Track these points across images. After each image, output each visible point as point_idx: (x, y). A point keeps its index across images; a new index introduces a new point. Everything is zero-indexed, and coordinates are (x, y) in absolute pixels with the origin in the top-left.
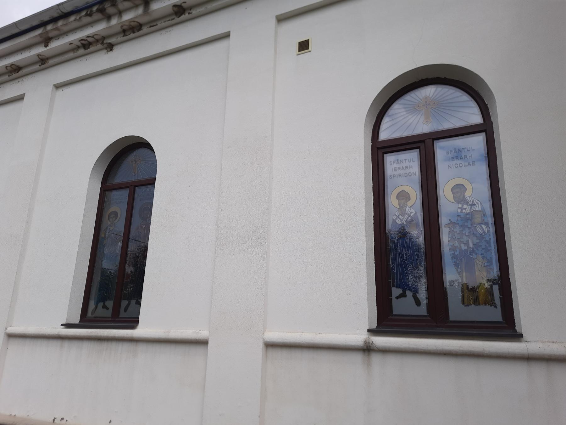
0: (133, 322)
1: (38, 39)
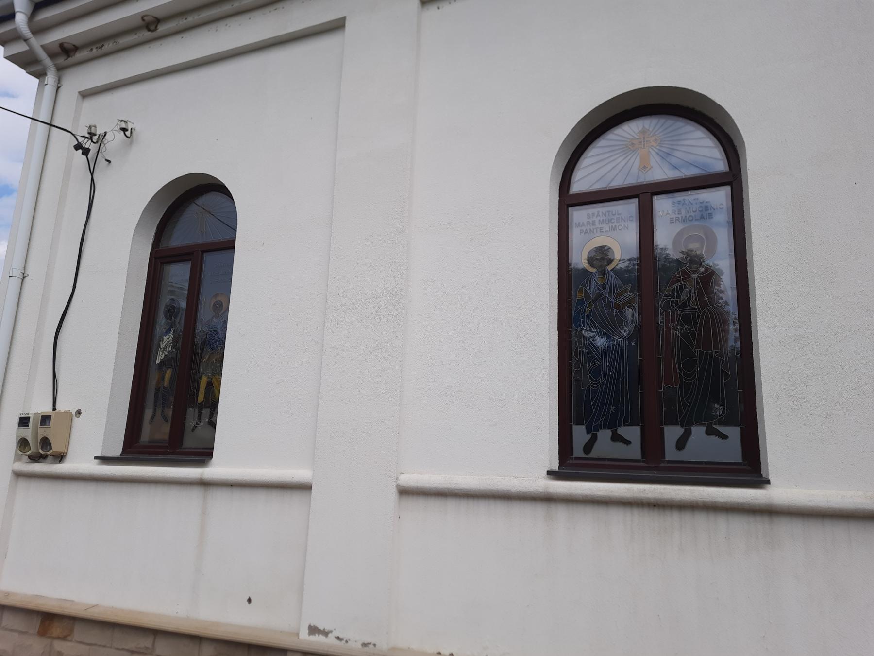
0: (203, 454)
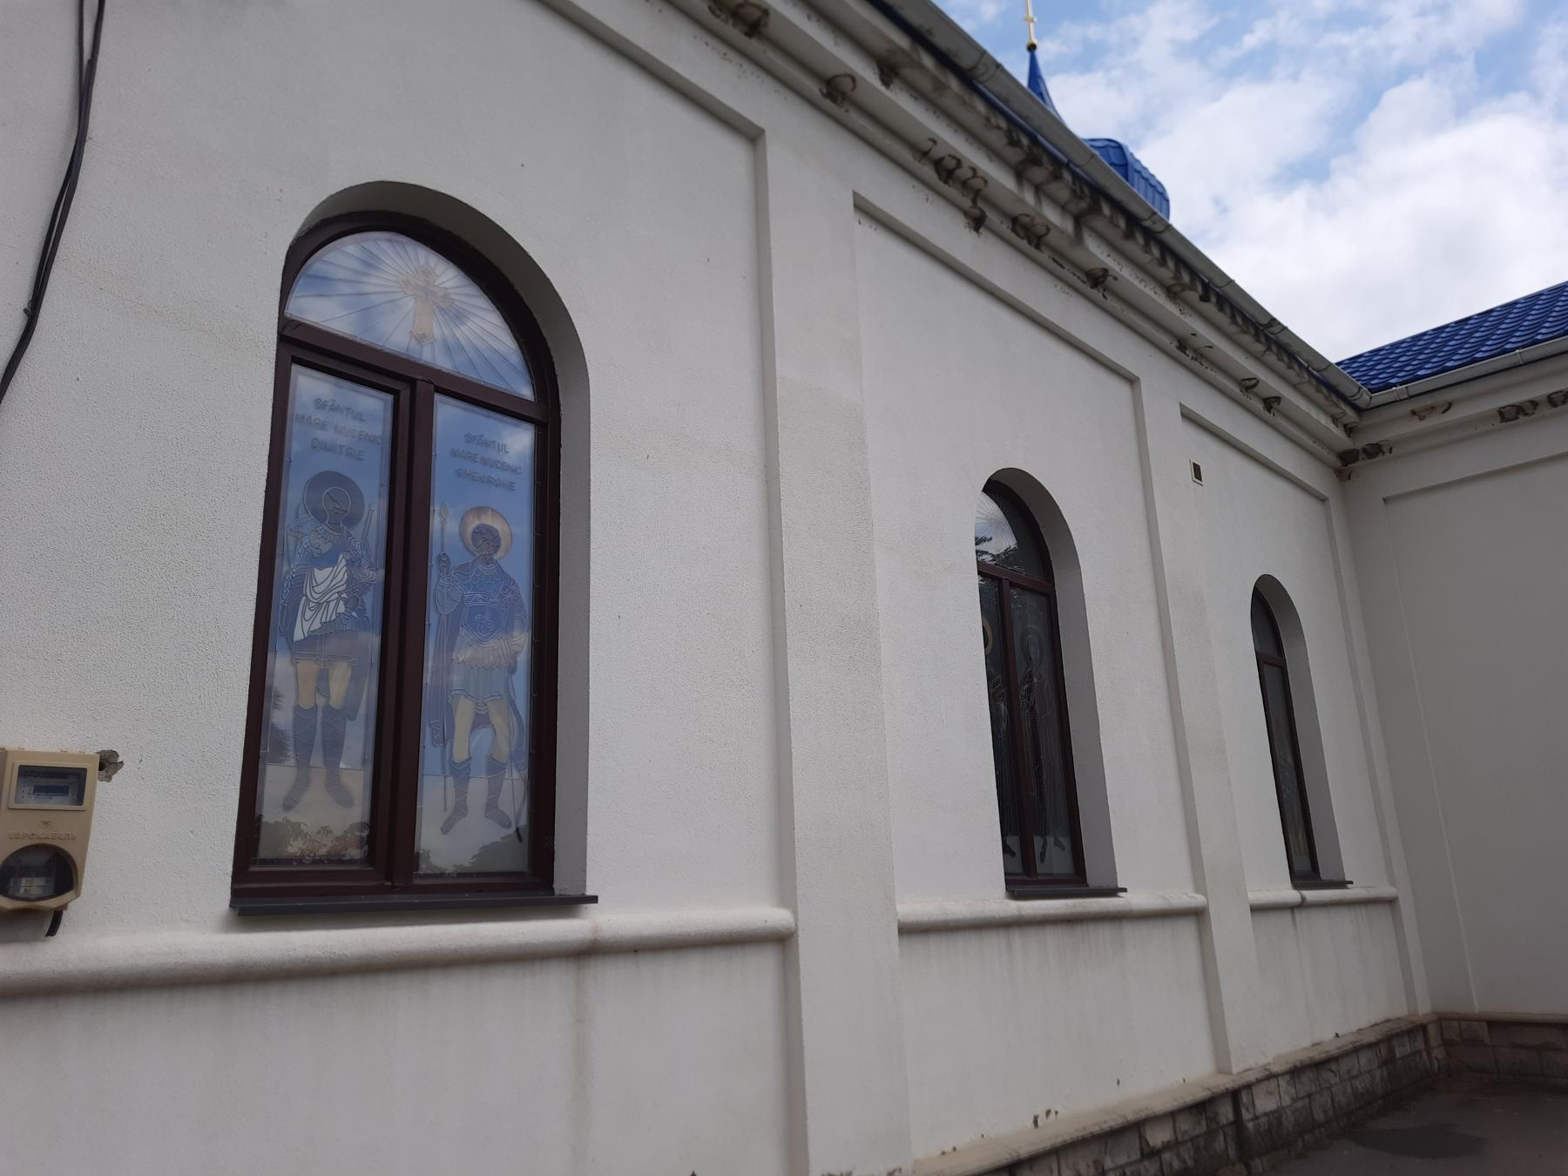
1: (881, 47)
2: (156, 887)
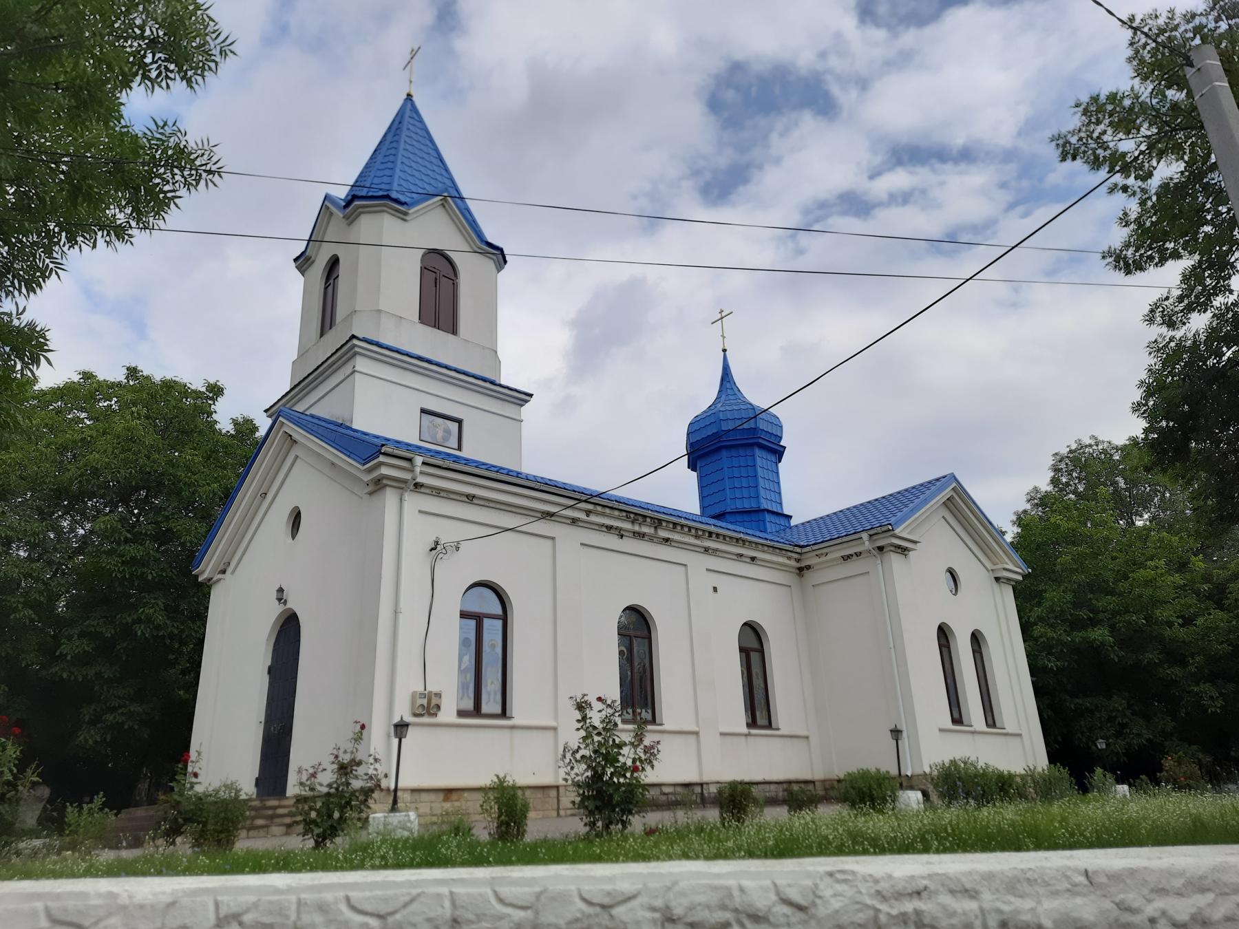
2: (448, 713)
